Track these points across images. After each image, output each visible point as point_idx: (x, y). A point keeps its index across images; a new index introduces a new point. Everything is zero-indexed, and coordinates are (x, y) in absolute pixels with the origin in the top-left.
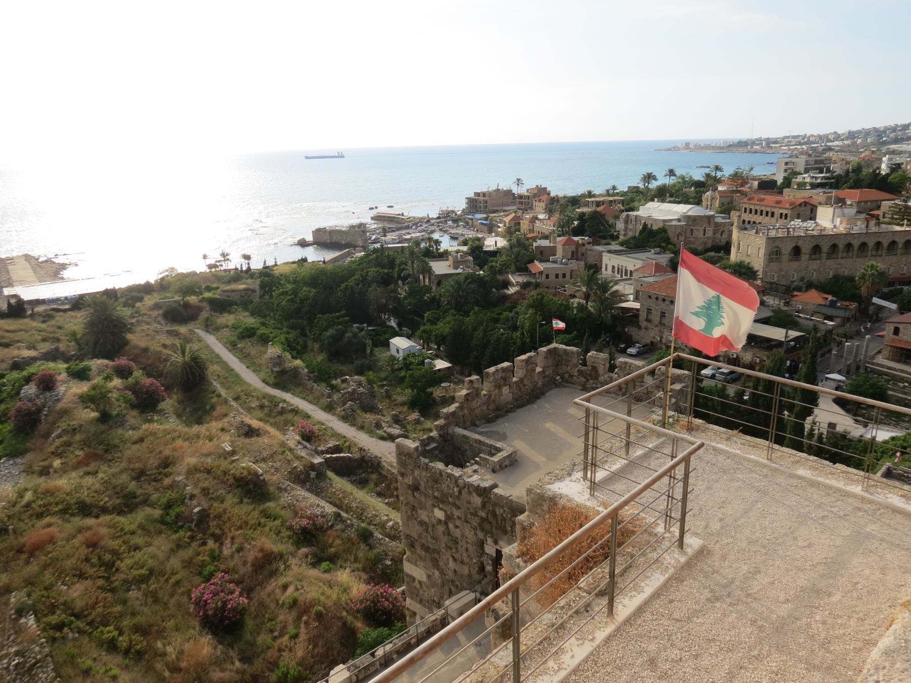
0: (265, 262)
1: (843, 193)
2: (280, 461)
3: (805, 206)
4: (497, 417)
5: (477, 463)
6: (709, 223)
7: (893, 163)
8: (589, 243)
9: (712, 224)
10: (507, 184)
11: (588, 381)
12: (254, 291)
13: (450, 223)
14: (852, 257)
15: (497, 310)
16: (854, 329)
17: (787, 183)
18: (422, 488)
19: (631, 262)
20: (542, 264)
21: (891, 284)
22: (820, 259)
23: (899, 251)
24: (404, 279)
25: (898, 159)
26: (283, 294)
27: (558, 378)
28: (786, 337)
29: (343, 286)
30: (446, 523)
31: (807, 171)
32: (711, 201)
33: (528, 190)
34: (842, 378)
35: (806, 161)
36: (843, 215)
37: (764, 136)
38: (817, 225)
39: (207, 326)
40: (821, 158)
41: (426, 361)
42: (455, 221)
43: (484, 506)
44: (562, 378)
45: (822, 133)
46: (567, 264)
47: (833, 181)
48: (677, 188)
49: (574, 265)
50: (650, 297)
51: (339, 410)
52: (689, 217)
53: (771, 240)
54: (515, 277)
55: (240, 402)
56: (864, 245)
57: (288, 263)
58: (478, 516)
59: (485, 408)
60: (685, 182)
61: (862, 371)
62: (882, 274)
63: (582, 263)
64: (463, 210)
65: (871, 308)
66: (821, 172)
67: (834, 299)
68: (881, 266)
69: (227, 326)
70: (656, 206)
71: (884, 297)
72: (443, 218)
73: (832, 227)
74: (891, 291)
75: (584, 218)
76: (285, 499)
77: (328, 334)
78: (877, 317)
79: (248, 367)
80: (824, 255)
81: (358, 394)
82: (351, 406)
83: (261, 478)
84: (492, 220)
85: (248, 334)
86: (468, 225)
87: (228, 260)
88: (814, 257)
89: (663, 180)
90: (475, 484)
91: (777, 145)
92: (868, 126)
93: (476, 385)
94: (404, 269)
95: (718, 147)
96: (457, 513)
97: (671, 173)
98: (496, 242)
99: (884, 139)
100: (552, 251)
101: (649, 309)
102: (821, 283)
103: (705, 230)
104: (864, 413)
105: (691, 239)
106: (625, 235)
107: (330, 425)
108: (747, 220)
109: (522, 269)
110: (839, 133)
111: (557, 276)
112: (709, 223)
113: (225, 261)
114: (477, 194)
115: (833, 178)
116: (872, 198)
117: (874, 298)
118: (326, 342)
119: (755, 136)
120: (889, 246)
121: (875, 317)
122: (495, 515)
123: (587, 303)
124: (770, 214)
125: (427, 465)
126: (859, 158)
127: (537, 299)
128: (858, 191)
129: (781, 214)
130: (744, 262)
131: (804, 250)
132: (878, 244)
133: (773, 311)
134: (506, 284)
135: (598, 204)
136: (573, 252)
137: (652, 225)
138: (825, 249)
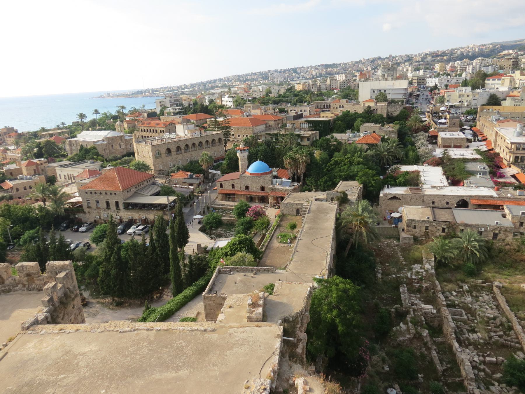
1: (188, 116)
3: (172, 125)
6: (122, 140)
8: (45, 162)
9: (123, 140)
14: (197, 150)
16: (203, 188)
17: (162, 113)
19: (76, 170)
20: (12, 182)
21: (216, 161)
23: (217, 144)
28: (168, 201)
31: (171, 106)
34: (202, 217)
35: (170, 101)
36: (188, 129)
38: (177, 135)
40: (177, 99)
45: (179, 85)
46: (31, 179)
47: (184, 110)
48: (103, 120)
49: (36, 178)
50: (86, 193)
52: (109, 138)
53: (153, 147)
60: (107, 116)
61: (211, 209)
63: (43, 177)
65: (210, 175)
66: (177, 106)
67: (191, 174)
68: (209, 154)
70: (87, 133)
71: (215, 168)
74: (217, 165)
75: (40, 146)
80: (183, 151)
88: (178, 153)
89: (90, 117)
91: (158, 92)
92: (199, 81)
100: (19, 171)
102: (184, 167)
103: (120, 145)
104: (215, 233)
105: (113, 151)
108: (144, 136)
110: (187, 85)
112: (122, 140)
115: (183, 109)
116: (203, 118)
119: (146, 88)
120: (212, 142)
123: (45, 204)
124: (155, 131)
126: (196, 97)
127: (5, 210)
129: (161, 130)
131: (172, 150)
132: (207, 141)
133: (161, 187)
135: (51, 135)
136: (35, 170)
137: (87, 146)
138: (183, 147)
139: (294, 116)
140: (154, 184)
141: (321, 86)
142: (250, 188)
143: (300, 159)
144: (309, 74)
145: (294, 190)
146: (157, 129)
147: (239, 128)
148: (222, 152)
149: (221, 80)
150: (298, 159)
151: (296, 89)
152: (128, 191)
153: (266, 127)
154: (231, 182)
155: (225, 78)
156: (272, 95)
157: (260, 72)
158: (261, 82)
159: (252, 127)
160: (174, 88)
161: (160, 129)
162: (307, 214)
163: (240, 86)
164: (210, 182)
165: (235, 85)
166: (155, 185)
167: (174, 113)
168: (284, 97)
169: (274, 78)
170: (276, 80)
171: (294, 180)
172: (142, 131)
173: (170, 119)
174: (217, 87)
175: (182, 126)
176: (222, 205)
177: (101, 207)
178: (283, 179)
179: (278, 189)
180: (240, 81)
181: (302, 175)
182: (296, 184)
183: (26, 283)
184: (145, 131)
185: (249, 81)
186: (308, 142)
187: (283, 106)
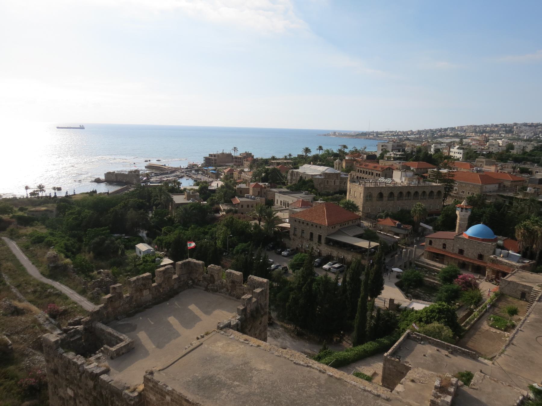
0: (67, 193)
2: (29, 334)
3: (389, 170)
4: (136, 312)
5: (102, 351)
6: (337, 178)
7: (436, 148)
8: (268, 187)
10: (228, 150)
11: (209, 284)
12: (51, 212)
13: (193, 172)
15: (208, 226)
17: (382, 157)
18: (60, 371)
19: (290, 199)
21: (430, 215)
22: (393, 200)
23: (435, 197)
24: (157, 205)
25: (439, 147)
26: (71, 214)
27: (190, 282)
28: (369, 246)
29: (112, 209)
30: (75, 400)
32: (339, 165)
33: (240, 154)
35: (393, 145)
36: (406, 176)
37: (375, 130)
38: (393, 181)
39: (11, 235)
40: (400, 144)
41: (157, 259)
42: (197, 171)
43: (95, 387)
44: (193, 282)
45: (405, 131)
47: (405, 156)
48: (324, 157)
50: (295, 221)
51: (89, 293)
52: (326, 174)
53: (366, 189)
54: (223, 207)
55: (20, 288)
56: (416, 193)
57: (83, 193)
58: (92, 395)
59: (127, 306)
61: (413, 265)
62: (424, 210)
63: (264, 199)
64: (202, 164)
65: (420, 229)
66: (399, 152)
69: (26, 235)
71: (427, 223)
72: (189, 168)
76: (26, 362)
77: (94, 241)
78: (422, 234)
79: (33, 264)
80: (396, 198)
81: (105, 282)
82: (97, 290)
83: (10, 347)
84: (218, 171)
85: (39, 240)
86: (205, 173)
87: (43, 190)
89: (314, 152)
90: (90, 371)
91: (382, 136)
92: (428, 128)
93: (118, 291)
94: (157, 199)
95: (351, 135)
96: (80, 392)
97: (320, 148)
98: (218, 184)
99: (435, 135)
101: (295, 228)
103: (335, 181)
105: (327, 186)
106: (291, 183)
107: (81, 304)
108: (359, 176)
109: (228, 202)
111: (248, 206)
112: (337, 178)
113: (41, 191)
114: (211, 155)
117: (421, 223)
118: (92, 246)
119: (371, 130)
121: (422, 234)
122: (101, 395)
124: (371, 174)
125: (61, 354)
127: (229, 221)
129: (377, 174)
130: (350, 201)
131: (384, 195)
132: (424, 192)
134: (218, 210)
135: (278, 164)
136: (259, 192)
138: (396, 194)
142: (465, 252)
145: (524, 268)
146: (374, 172)
147: (464, 183)
148: (438, 206)
149: (453, 129)
152: (332, 228)
153: (499, 187)
155: (458, 127)
158: (503, 135)
159: (480, 184)
162: (535, 302)
163: (474, 138)
168: (530, 155)
169: (521, 132)
170: (523, 134)
172: (358, 172)
173: (388, 164)
174: (447, 136)
175: (400, 173)
178: (510, 252)
180: (476, 132)
181: (538, 252)
183: (229, 288)
185: (486, 132)
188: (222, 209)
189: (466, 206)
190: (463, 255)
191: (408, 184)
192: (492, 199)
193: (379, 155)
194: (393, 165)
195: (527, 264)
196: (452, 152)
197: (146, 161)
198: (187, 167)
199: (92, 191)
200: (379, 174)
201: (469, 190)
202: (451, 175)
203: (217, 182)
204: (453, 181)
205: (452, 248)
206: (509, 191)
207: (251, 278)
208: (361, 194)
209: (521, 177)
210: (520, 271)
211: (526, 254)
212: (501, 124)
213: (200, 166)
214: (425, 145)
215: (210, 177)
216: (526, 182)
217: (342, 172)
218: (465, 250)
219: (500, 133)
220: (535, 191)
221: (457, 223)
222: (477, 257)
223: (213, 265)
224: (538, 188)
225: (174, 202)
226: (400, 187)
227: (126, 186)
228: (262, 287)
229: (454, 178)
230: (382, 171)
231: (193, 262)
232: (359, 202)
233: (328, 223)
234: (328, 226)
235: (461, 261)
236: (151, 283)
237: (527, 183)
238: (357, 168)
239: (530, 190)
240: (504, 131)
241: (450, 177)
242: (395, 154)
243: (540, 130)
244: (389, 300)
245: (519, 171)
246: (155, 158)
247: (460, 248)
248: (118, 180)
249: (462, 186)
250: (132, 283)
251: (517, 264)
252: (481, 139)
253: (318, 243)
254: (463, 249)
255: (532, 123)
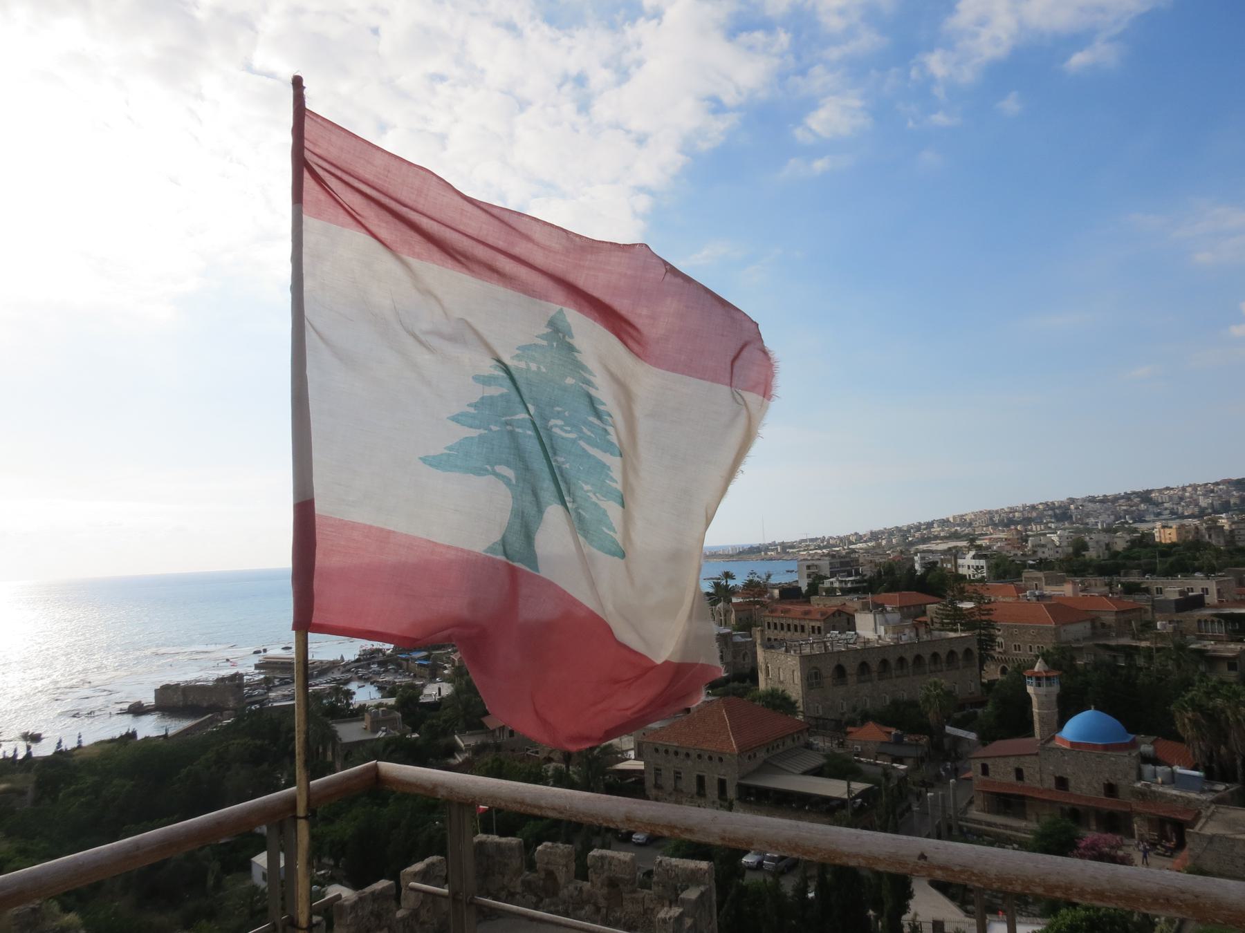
0: (60, 743)
1: (882, 597)
3: (840, 616)
12: (22, 793)
13: (374, 667)
17: (813, 589)
21: (961, 707)
23: (961, 664)
28: (849, 792)
29: (184, 771)
31: (833, 575)
32: (725, 615)
35: (831, 564)
36: (886, 622)
38: (858, 636)
47: (865, 584)
50: (657, 750)
53: (805, 660)
56: (918, 658)
65: (946, 741)
66: (850, 575)
67: (899, 732)
68: (945, 683)
71: (958, 724)
73: (877, 637)
80: (875, 675)
91: (794, 550)
95: (727, 555)
98: (440, 689)
99: (910, 539)
119: (768, 541)
123: (568, 767)
124: (799, 628)
128: (897, 594)
129: (813, 627)
132: (935, 656)
138: (874, 665)
139: (1177, 601)
140: (809, 746)
141: (1236, 532)
142: (1072, 783)
143: (1229, 713)
144: (1188, 506)
145: (1219, 801)
146: (805, 623)
147: (1015, 627)
148: (973, 684)
149: (944, 523)
150: (1223, 711)
151: (1157, 540)
152: (750, 757)
153: (1094, 627)
154: (1013, 763)
155: (954, 518)
156: (1091, 554)
157: (1046, 504)
158: (1053, 526)
159: (1053, 625)
160: (831, 542)
161: (813, 624)
163: (994, 536)
164: (948, 761)
165: (982, 535)
166: (812, 749)
167: (842, 589)
168: (1127, 557)
169: (1088, 515)
170: (1092, 520)
171: (1211, 776)
172: (769, 627)
173: (835, 602)
174: (936, 538)
175: (870, 617)
176: (989, 824)
177: (685, 790)
178: (1179, 770)
179: (1163, 795)
180: (995, 525)
181: (1239, 762)
182: (1220, 787)
183: (602, 903)
184: (776, 628)
185: (1017, 523)
186: (1233, 673)
187: (1134, 578)
188: (462, 745)
189: (1045, 672)
190: (1068, 790)
191: (895, 641)
192: (1085, 656)
193: (807, 588)
194: (845, 604)
195: (1223, 793)
196: (963, 566)
197: (256, 652)
198: (357, 657)
199: (124, 733)
200: (819, 628)
201: (1030, 642)
202: (986, 610)
203: (436, 686)
204: (990, 625)
205: (1038, 777)
206: (1116, 635)
207: (664, 864)
208: (795, 673)
209: (1131, 601)
210: (1221, 810)
211: (1215, 771)
212: (1041, 504)
213: (389, 652)
214: (896, 560)
215: (415, 676)
216: (1146, 611)
217: (734, 630)
218: (1069, 777)
219: (1045, 521)
220: (1175, 628)
221: (1034, 714)
222: (1103, 791)
223: (549, 844)
224: (1178, 622)
225: (340, 739)
226: (877, 647)
227: (210, 715)
228: (698, 885)
229: (993, 618)
230: (824, 620)
231: (491, 843)
232: (794, 689)
233: (738, 747)
234: (739, 755)
235: (1067, 807)
236: (395, 908)
237: (1150, 614)
238: (767, 619)
239: (1164, 626)
240: (1051, 516)
241: (983, 615)
242: (841, 582)
243: (1125, 508)
244: (931, 926)
245: (1121, 591)
246: (278, 643)
247: (1057, 775)
248: (189, 703)
249: (1012, 634)
250: (349, 911)
251: (1203, 797)
252: (1011, 537)
253: (718, 801)
254: (1065, 776)
255: (1105, 496)
